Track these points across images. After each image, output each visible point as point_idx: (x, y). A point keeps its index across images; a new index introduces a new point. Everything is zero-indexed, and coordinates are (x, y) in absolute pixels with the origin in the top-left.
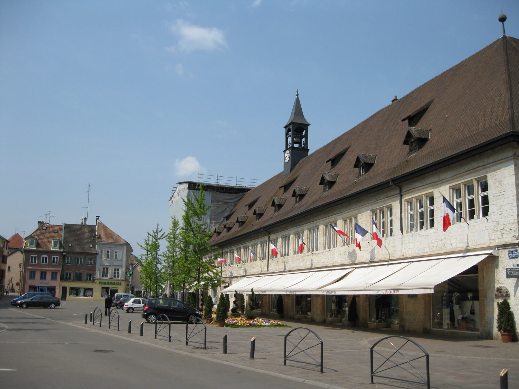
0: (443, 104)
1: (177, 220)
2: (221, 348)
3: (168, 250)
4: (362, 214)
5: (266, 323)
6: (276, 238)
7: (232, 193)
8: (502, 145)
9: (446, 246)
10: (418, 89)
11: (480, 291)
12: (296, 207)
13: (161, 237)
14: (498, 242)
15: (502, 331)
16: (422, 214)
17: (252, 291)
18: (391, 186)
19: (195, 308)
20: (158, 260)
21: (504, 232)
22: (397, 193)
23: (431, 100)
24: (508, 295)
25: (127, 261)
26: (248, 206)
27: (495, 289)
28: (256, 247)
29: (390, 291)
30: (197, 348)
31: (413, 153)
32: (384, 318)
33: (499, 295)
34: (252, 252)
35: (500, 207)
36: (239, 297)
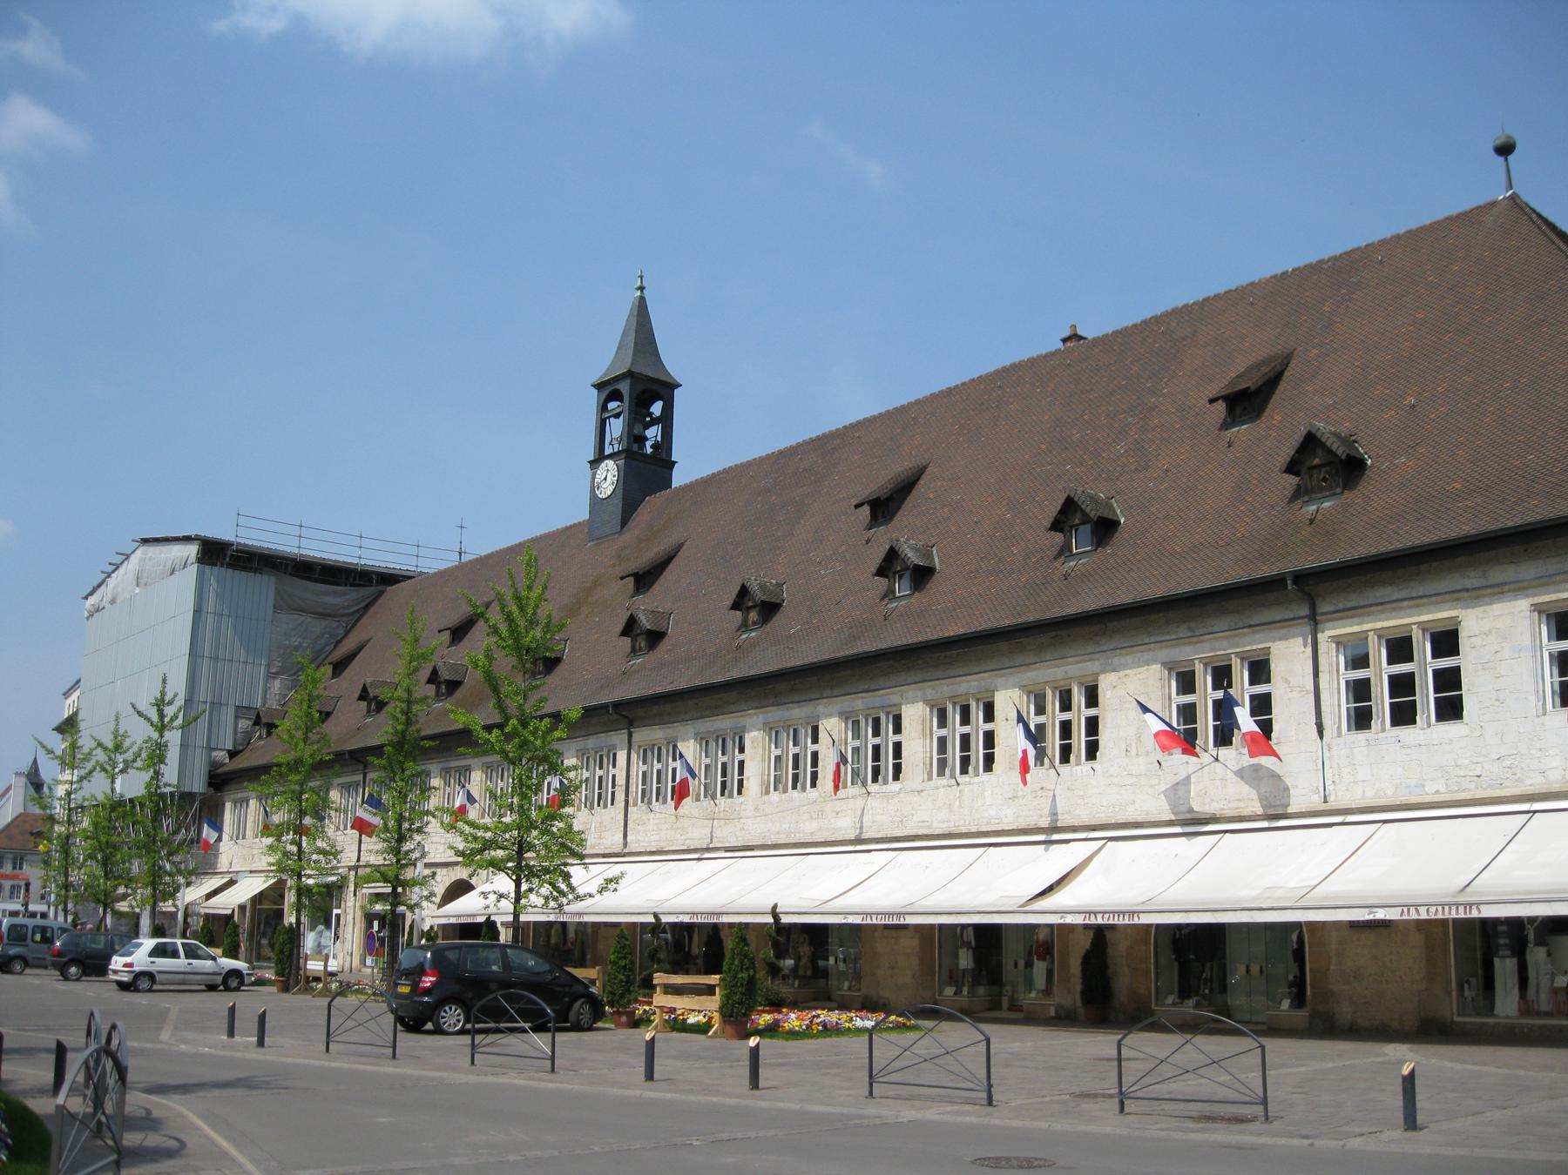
9: (1518, 775)
32: (1207, 991)
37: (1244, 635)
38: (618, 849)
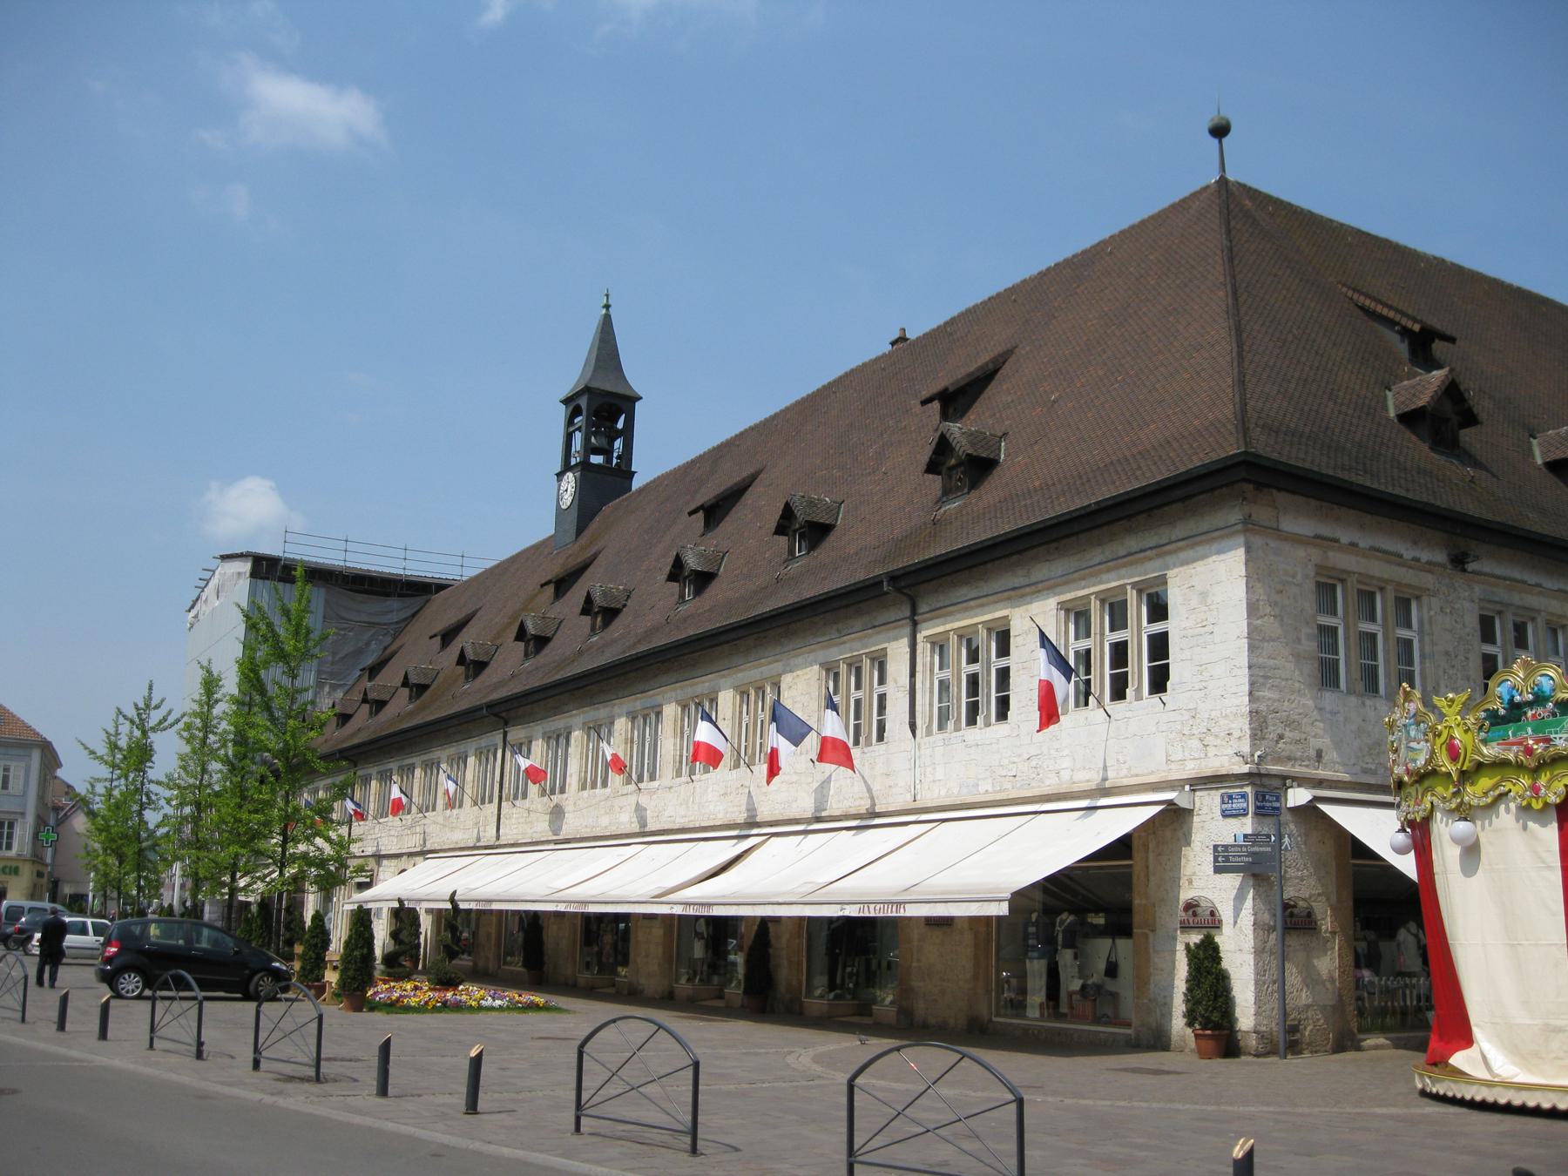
0: (1043, 362)
1: (215, 674)
2: (371, 1079)
3: (184, 768)
4: (795, 674)
5: (494, 1001)
6: (525, 737)
7: (388, 595)
8: (1212, 490)
10: (969, 312)
11: (1136, 909)
12: (590, 648)
13: (161, 726)
14: (1191, 770)
15: (1198, 1027)
16: (973, 681)
17: (452, 900)
18: (887, 593)
19: (268, 950)
20: (148, 797)
21: (1210, 740)
22: (902, 617)
23: (1009, 345)
24: (1217, 922)
25: (41, 798)
26: (439, 638)
27: (1181, 903)
28: (462, 765)
29: (878, 908)
30: (290, 1079)
31: (954, 500)
32: (851, 985)
33: (1191, 921)
34: (449, 777)
35: (1199, 668)
36: (404, 917)
37: (870, 636)
38: (492, 841)
